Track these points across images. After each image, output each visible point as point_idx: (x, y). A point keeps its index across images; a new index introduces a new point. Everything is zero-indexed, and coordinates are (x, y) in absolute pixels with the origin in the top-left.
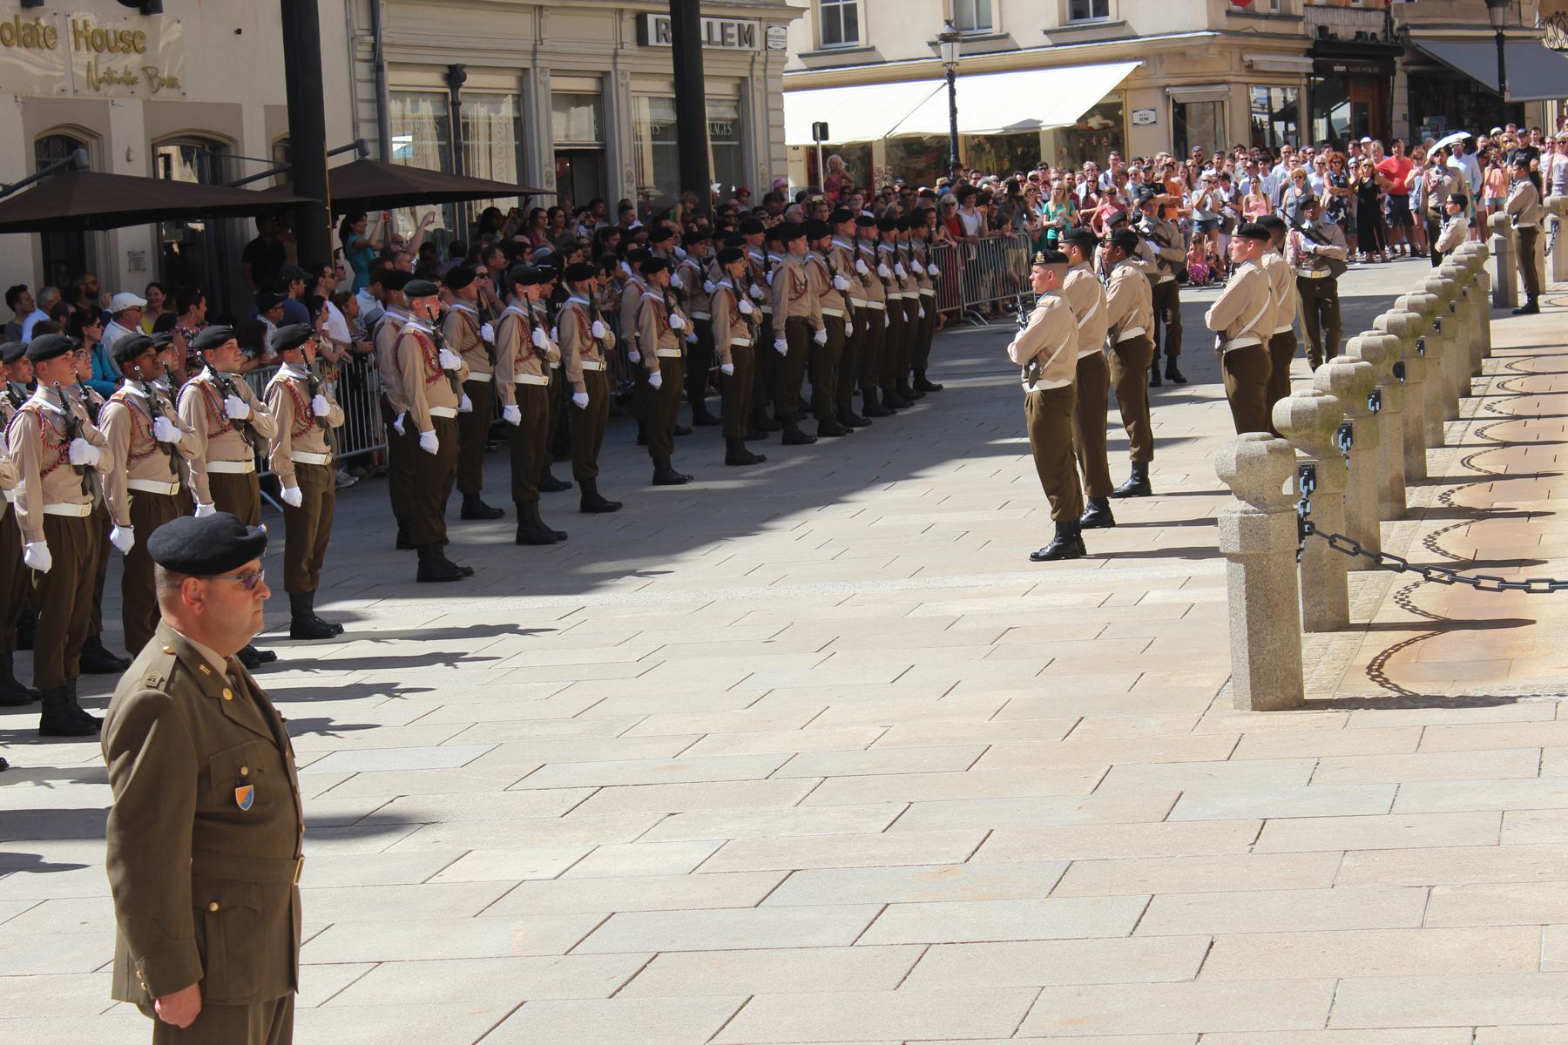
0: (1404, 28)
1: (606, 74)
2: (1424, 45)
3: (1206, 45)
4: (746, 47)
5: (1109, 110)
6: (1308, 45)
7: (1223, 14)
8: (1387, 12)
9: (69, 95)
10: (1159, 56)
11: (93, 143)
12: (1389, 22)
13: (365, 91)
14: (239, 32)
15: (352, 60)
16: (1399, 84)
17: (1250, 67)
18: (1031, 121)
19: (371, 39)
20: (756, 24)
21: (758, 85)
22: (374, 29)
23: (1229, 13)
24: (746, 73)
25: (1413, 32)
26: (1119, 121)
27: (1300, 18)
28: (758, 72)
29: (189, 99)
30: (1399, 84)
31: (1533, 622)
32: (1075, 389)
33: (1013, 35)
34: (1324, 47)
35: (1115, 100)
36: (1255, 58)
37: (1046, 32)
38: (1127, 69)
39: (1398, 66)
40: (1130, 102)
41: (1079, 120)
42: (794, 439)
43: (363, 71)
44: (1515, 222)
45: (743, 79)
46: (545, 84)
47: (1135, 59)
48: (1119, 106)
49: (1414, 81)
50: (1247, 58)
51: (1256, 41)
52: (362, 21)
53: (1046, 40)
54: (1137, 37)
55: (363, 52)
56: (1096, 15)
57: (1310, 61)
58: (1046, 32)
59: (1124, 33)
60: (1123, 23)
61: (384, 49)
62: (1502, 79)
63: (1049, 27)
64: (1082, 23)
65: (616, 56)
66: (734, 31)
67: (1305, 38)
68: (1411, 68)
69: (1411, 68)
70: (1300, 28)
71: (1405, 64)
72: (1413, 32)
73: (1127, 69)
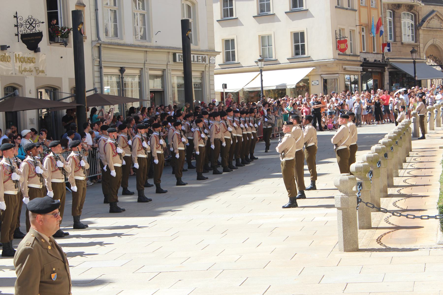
0: (388, 59)
1: (164, 70)
3: (333, 63)
4: (204, 63)
6: (361, 63)
8: (383, 54)
9: (14, 75)
10: (319, 65)
11: (20, 88)
12: (383, 57)
13: (97, 74)
14: (62, 57)
15: (93, 65)
16: (386, 74)
17: (345, 69)
19: (99, 60)
21: (207, 73)
22: (100, 57)
23: (339, 54)
24: (204, 70)
25: (390, 60)
26: (308, 84)
27: (359, 56)
28: (207, 69)
29: (47, 76)
30: (386, 74)
32: (295, 160)
33: (279, 60)
34: (365, 64)
35: (307, 78)
36: (346, 67)
37: (288, 59)
38: (310, 69)
39: (386, 69)
40: (311, 79)
41: (297, 84)
43: (96, 68)
45: (203, 71)
46: (147, 73)
47: (313, 67)
48: (308, 80)
49: (390, 73)
50: (344, 67)
52: (96, 55)
53: (288, 61)
54: (313, 61)
55: (97, 63)
56: (302, 54)
57: (362, 68)
58: (288, 59)
60: (309, 57)
61: (103, 63)
62: (415, 73)
63: (289, 57)
64: (298, 56)
65: (167, 65)
66: (200, 58)
67: (360, 61)
68: (390, 70)
69: (390, 70)
70: (359, 59)
72: (390, 60)
73: (310, 69)
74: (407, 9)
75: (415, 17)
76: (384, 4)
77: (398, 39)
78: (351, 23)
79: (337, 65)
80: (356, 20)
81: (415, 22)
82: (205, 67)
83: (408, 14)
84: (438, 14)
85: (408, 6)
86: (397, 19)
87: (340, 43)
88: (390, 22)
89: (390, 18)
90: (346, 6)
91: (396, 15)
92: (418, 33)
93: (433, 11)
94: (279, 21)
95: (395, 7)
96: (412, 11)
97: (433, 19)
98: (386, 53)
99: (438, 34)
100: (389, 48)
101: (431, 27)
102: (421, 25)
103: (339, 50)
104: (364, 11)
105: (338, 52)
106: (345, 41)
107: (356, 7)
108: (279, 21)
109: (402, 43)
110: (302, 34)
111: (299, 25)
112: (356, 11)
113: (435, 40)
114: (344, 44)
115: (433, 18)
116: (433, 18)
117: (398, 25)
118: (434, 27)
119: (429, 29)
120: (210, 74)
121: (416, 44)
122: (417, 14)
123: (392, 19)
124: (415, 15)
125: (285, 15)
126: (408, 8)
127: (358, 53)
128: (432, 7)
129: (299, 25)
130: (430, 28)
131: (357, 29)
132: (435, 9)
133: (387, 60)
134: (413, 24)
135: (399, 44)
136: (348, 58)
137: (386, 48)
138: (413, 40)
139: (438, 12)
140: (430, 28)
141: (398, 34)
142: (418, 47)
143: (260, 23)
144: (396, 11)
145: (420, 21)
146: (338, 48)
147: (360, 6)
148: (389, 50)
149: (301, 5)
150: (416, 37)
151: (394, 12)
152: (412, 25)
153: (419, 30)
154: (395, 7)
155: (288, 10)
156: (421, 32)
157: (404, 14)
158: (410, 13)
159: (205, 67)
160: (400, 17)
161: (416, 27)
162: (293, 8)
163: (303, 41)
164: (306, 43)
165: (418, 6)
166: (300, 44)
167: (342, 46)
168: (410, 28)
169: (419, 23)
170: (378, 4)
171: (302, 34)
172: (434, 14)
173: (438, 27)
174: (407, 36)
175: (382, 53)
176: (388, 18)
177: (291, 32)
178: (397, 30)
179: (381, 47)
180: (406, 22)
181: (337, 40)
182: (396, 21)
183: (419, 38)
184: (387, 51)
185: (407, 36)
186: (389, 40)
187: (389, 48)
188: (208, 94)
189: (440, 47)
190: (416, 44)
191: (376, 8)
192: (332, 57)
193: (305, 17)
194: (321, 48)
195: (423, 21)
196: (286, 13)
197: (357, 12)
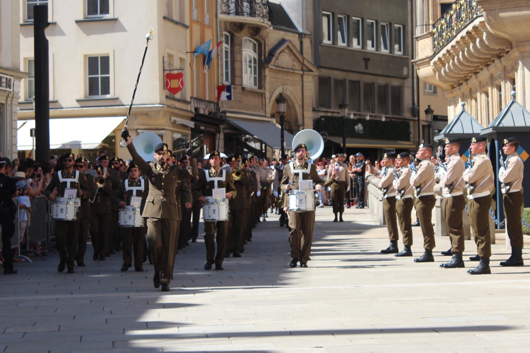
0: (224, 112)
2: (230, 119)
4: (8, 89)
5: (109, 140)
6: (192, 115)
7: (164, 97)
8: (218, 104)
12: (218, 108)
18: (75, 141)
20: (12, 78)
21: (9, 108)
23: (167, 97)
24: (4, 102)
26: (114, 144)
28: (9, 102)
31: (81, 341)
33: (60, 101)
34: (197, 117)
35: (113, 135)
37: (78, 101)
39: (221, 130)
41: (105, 141)
42: (109, 256)
44: (472, 192)
47: (123, 115)
49: (228, 139)
50: (173, 118)
51: (176, 111)
53: (77, 105)
54: (123, 105)
56: (102, 94)
58: (78, 101)
59: (117, 103)
60: (117, 99)
62: (282, 136)
64: (96, 97)
67: (191, 112)
68: (226, 131)
69: (226, 131)
70: (189, 107)
71: (223, 129)
72: (228, 115)
74: (250, 33)
75: (259, 47)
76: (220, 22)
77: (237, 81)
78: (182, 45)
79: (164, 115)
80: (186, 42)
81: (260, 55)
82: (7, 98)
83: (251, 41)
84: (290, 46)
85: (252, 28)
86: (237, 48)
87: (171, 79)
88: (226, 52)
89: (226, 45)
90: (176, 18)
91: (236, 41)
92: (263, 74)
93: (283, 41)
94: (62, 33)
95: (235, 28)
96: (256, 37)
97: (283, 54)
98: (222, 102)
99: (288, 77)
100: (228, 94)
101: (280, 65)
102: (268, 61)
103: (169, 90)
104: (196, 29)
105: (167, 92)
106: (179, 76)
107: (187, 23)
108: (62, 33)
109: (243, 89)
110: (105, 60)
111: (99, 44)
112: (186, 27)
113: (285, 87)
114: (177, 80)
115: (283, 51)
116: (283, 51)
117: (237, 57)
118: (285, 66)
119: (278, 69)
120: (13, 110)
121: (261, 91)
122: (263, 42)
123: (229, 47)
124: (260, 44)
125: (76, 26)
126: (252, 32)
127: (188, 99)
128: (282, 33)
129: (99, 44)
130: (278, 67)
131: (188, 58)
132: (286, 38)
133: (223, 115)
134: (257, 58)
135: (239, 89)
136: (178, 105)
137: (224, 94)
138: (255, 84)
139: (290, 42)
140: (278, 67)
141: (237, 72)
142: (264, 96)
143: (88, 33)
144: (236, 34)
145: (267, 54)
146: (166, 85)
147: (191, 21)
148: (229, 98)
149: (105, 9)
150: (260, 81)
151: (232, 36)
152: (255, 59)
153: (264, 68)
154: (235, 28)
155: (81, 18)
156: (267, 72)
157: (246, 39)
158: (253, 40)
159: (7, 98)
160: (241, 45)
161: (263, 61)
162: (88, 14)
163: (106, 69)
164: (111, 75)
165: (266, 28)
166: (100, 76)
167: (175, 83)
168: (253, 65)
169: (265, 58)
170: (213, 21)
171: (105, 60)
172: (285, 45)
173: (290, 66)
174: (248, 79)
175: (216, 101)
176: (225, 46)
177: (85, 56)
178: (237, 65)
179: (216, 91)
180: (248, 52)
181: (167, 72)
182: (235, 51)
183: (265, 82)
184: (226, 99)
185: (248, 79)
186: (226, 83)
187: (228, 94)
188: (8, 145)
189: (291, 99)
190: (261, 91)
191: (210, 26)
192: (159, 102)
193: (112, 31)
194: (138, 83)
195: (271, 54)
196: (77, 22)
197: (188, 30)
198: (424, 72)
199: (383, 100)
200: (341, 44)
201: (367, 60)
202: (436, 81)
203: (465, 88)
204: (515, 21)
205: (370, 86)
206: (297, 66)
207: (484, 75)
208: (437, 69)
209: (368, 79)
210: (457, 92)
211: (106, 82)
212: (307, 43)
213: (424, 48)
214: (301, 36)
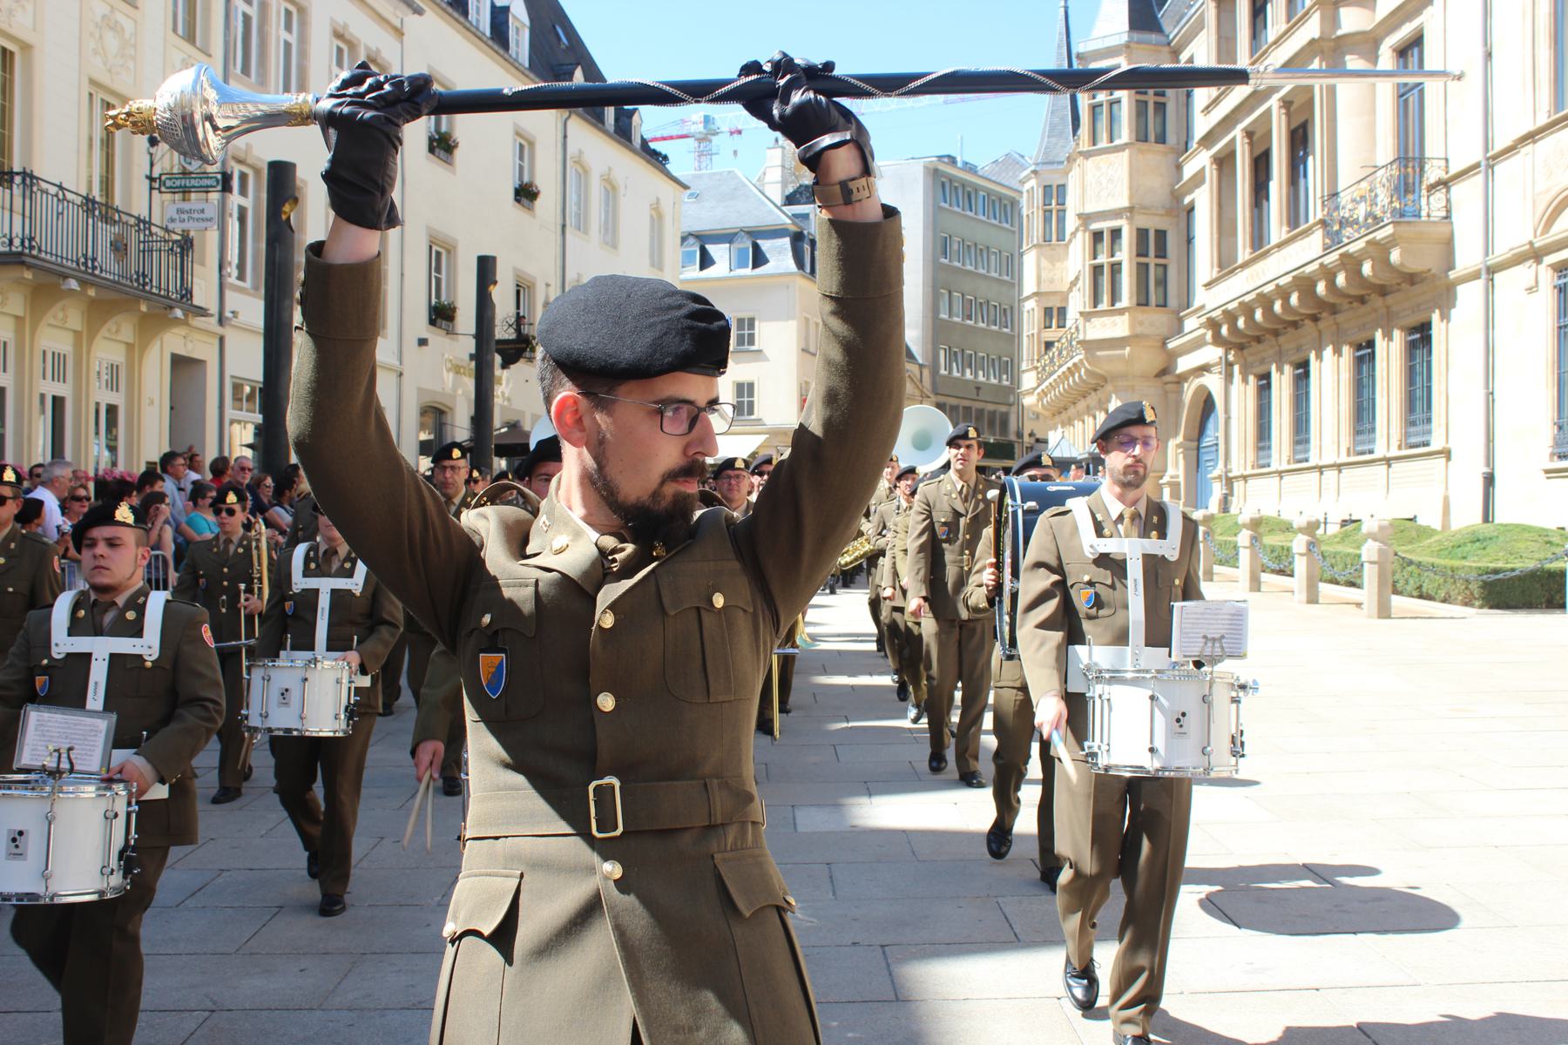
73: (763, 438)
110: (751, 386)
163: (751, 394)
164: (755, 399)
171: (751, 386)
198: (1028, 401)
199: (991, 424)
200: (956, 374)
201: (978, 389)
202: (1039, 408)
203: (1064, 416)
204: (1110, 359)
205: (980, 412)
206: (917, 393)
207: (1082, 405)
208: (1040, 399)
209: (979, 405)
210: (1057, 418)
211: (751, 404)
212: (926, 373)
213: (1028, 380)
214: (921, 366)
